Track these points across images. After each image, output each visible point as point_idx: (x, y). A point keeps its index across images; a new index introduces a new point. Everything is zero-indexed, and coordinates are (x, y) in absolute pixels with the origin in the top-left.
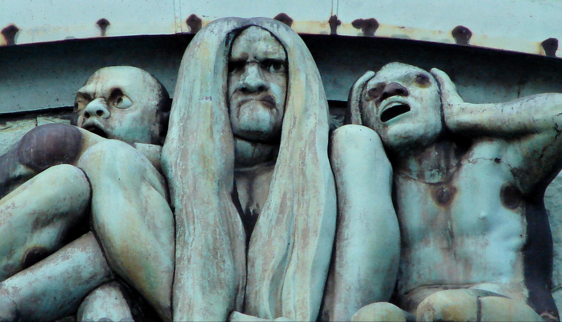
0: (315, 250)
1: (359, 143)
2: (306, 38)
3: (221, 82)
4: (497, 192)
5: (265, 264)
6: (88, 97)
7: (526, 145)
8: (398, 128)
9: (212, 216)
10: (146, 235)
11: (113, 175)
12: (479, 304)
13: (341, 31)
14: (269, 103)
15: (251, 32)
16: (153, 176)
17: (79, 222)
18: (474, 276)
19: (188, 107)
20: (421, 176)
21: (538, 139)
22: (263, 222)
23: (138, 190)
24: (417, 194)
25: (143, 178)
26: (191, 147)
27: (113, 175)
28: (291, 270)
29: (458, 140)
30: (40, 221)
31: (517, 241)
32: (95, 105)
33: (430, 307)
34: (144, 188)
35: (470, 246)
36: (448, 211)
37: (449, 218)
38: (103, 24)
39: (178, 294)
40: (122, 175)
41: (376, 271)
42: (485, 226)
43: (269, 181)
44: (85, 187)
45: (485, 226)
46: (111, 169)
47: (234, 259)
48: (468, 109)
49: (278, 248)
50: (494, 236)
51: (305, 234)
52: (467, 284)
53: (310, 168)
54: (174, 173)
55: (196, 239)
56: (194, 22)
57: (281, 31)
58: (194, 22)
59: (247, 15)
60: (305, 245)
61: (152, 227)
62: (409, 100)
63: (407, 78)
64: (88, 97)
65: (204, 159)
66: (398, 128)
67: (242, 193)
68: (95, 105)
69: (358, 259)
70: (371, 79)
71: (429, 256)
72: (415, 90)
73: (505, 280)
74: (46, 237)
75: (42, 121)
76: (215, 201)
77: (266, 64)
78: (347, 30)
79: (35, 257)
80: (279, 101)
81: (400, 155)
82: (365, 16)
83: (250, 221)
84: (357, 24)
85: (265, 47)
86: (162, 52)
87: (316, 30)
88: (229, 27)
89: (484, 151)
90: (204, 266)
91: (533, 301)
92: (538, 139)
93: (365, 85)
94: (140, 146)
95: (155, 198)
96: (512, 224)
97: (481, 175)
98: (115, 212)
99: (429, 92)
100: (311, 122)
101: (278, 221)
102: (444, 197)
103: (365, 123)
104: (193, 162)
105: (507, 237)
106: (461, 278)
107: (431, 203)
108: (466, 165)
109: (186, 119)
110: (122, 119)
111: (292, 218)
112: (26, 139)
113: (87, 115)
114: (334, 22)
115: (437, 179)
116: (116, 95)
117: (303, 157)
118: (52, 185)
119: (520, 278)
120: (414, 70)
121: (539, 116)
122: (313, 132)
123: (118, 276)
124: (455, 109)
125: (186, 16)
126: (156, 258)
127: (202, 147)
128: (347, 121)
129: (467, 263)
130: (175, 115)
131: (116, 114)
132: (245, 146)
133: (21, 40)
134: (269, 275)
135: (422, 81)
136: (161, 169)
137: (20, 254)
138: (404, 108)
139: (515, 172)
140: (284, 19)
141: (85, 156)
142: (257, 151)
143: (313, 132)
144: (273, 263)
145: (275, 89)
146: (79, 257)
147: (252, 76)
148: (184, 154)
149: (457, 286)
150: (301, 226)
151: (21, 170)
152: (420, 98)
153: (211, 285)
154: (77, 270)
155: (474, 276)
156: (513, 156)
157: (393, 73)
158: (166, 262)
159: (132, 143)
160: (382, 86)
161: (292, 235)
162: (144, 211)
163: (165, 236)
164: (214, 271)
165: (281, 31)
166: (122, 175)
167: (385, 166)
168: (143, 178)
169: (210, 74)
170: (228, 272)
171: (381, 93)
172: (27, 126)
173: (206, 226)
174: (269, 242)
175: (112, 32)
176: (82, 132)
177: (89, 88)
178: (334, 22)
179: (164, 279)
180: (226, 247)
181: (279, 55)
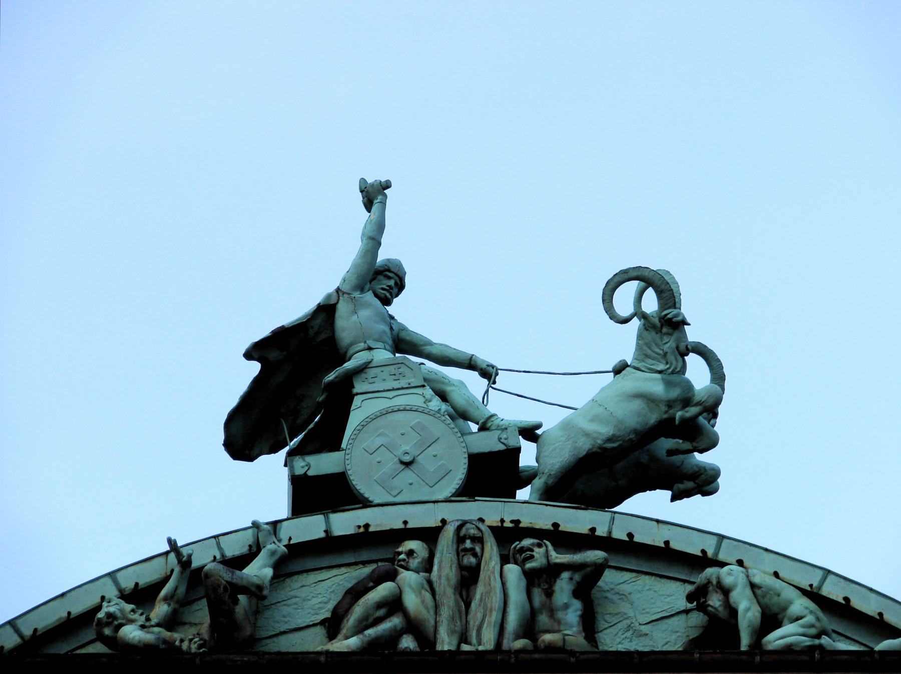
0: (495, 616)
1: (513, 571)
2: (490, 527)
3: (455, 546)
4: (571, 592)
5: (475, 622)
6: (400, 553)
7: (583, 572)
8: (529, 565)
9: (452, 603)
10: (424, 611)
11: (410, 586)
12: (564, 639)
13: (505, 525)
14: (475, 555)
15: (468, 525)
16: (426, 586)
17: (394, 605)
18: (562, 628)
19: (441, 557)
20: (539, 586)
21: (589, 569)
22: (473, 605)
23: (420, 593)
24: (538, 597)
25: (423, 588)
26: (443, 574)
27: (410, 586)
28: (485, 625)
29: (552, 571)
30: (379, 605)
31: (579, 613)
32: (402, 556)
33: (543, 641)
34: (423, 592)
35: (560, 615)
36: (551, 600)
37: (551, 603)
38: (405, 523)
39: (438, 636)
40: (414, 586)
41: (521, 626)
42: (566, 606)
43: (476, 588)
44: (398, 591)
45: (566, 606)
46: (409, 578)
47: (461, 621)
48: (558, 558)
49: (479, 616)
50: (570, 610)
51: (491, 610)
52: (558, 631)
53: (492, 583)
54: (436, 585)
55: (445, 613)
56: (444, 522)
57: (480, 525)
58: (444, 522)
59: (466, 518)
60: (491, 616)
61: (426, 608)
62: (534, 554)
63: (533, 544)
64: (400, 553)
65: (448, 579)
66: (529, 565)
67: (464, 593)
68: (402, 556)
69: (513, 620)
70: (517, 545)
71: (543, 619)
72: (537, 550)
73: (575, 629)
74: (381, 612)
75: (380, 564)
76: (453, 597)
77: (474, 539)
78: (507, 524)
79: (378, 621)
80: (479, 554)
81: (532, 578)
82: (515, 518)
83: (468, 605)
84: (512, 522)
85: (473, 532)
86: (429, 536)
87: (495, 524)
88: (457, 524)
89: (566, 575)
90: (448, 625)
91: (586, 638)
92: (589, 569)
93: (515, 547)
94: (421, 574)
95: (428, 596)
96: (577, 605)
97: (564, 586)
98: (411, 601)
99: (542, 550)
100: (493, 563)
101: (480, 605)
102: (549, 594)
103: (516, 563)
104: (443, 581)
105: (576, 611)
106: (556, 628)
107: (544, 597)
108: (558, 581)
109: (440, 562)
110: (414, 563)
111: (485, 604)
112: (373, 571)
113: (399, 561)
114: (502, 521)
115: (546, 587)
116: (411, 553)
117: (489, 578)
118: (384, 589)
119: (581, 628)
120: (536, 541)
121: (588, 560)
122: (494, 568)
123: (413, 626)
124: (553, 557)
125: (440, 519)
126: (429, 621)
127: (447, 575)
128: (509, 563)
129: (559, 622)
130: (436, 561)
131: (411, 561)
132: (465, 573)
133: (371, 529)
134: (476, 628)
135: (539, 546)
136: (430, 583)
137: (371, 620)
138: (532, 557)
139: (578, 583)
140: (481, 520)
141: (399, 578)
142: (468, 578)
143: (494, 568)
144: (477, 623)
145: (478, 549)
146: (396, 621)
147: (468, 544)
148: (440, 577)
149: (554, 632)
150: (489, 605)
151: (371, 584)
152: (538, 552)
153: (452, 632)
154: (395, 627)
155: (562, 628)
156: (577, 577)
157: (527, 542)
158: (432, 622)
159: (418, 572)
160: (522, 548)
161: (485, 611)
162: (423, 602)
163: (432, 612)
164: (452, 626)
165: (480, 525)
166: (414, 586)
167: (524, 582)
168: (423, 588)
169: (450, 543)
170: (458, 627)
171: (522, 550)
172: (374, 566)
173: (449, 607)
174: (476, 614)
175: (410, 526)
176: (449, 382)
177: (400, 549)
178: (502, 521)
179: (432, 630)
180: (457, 616)
181: (479, 535)
